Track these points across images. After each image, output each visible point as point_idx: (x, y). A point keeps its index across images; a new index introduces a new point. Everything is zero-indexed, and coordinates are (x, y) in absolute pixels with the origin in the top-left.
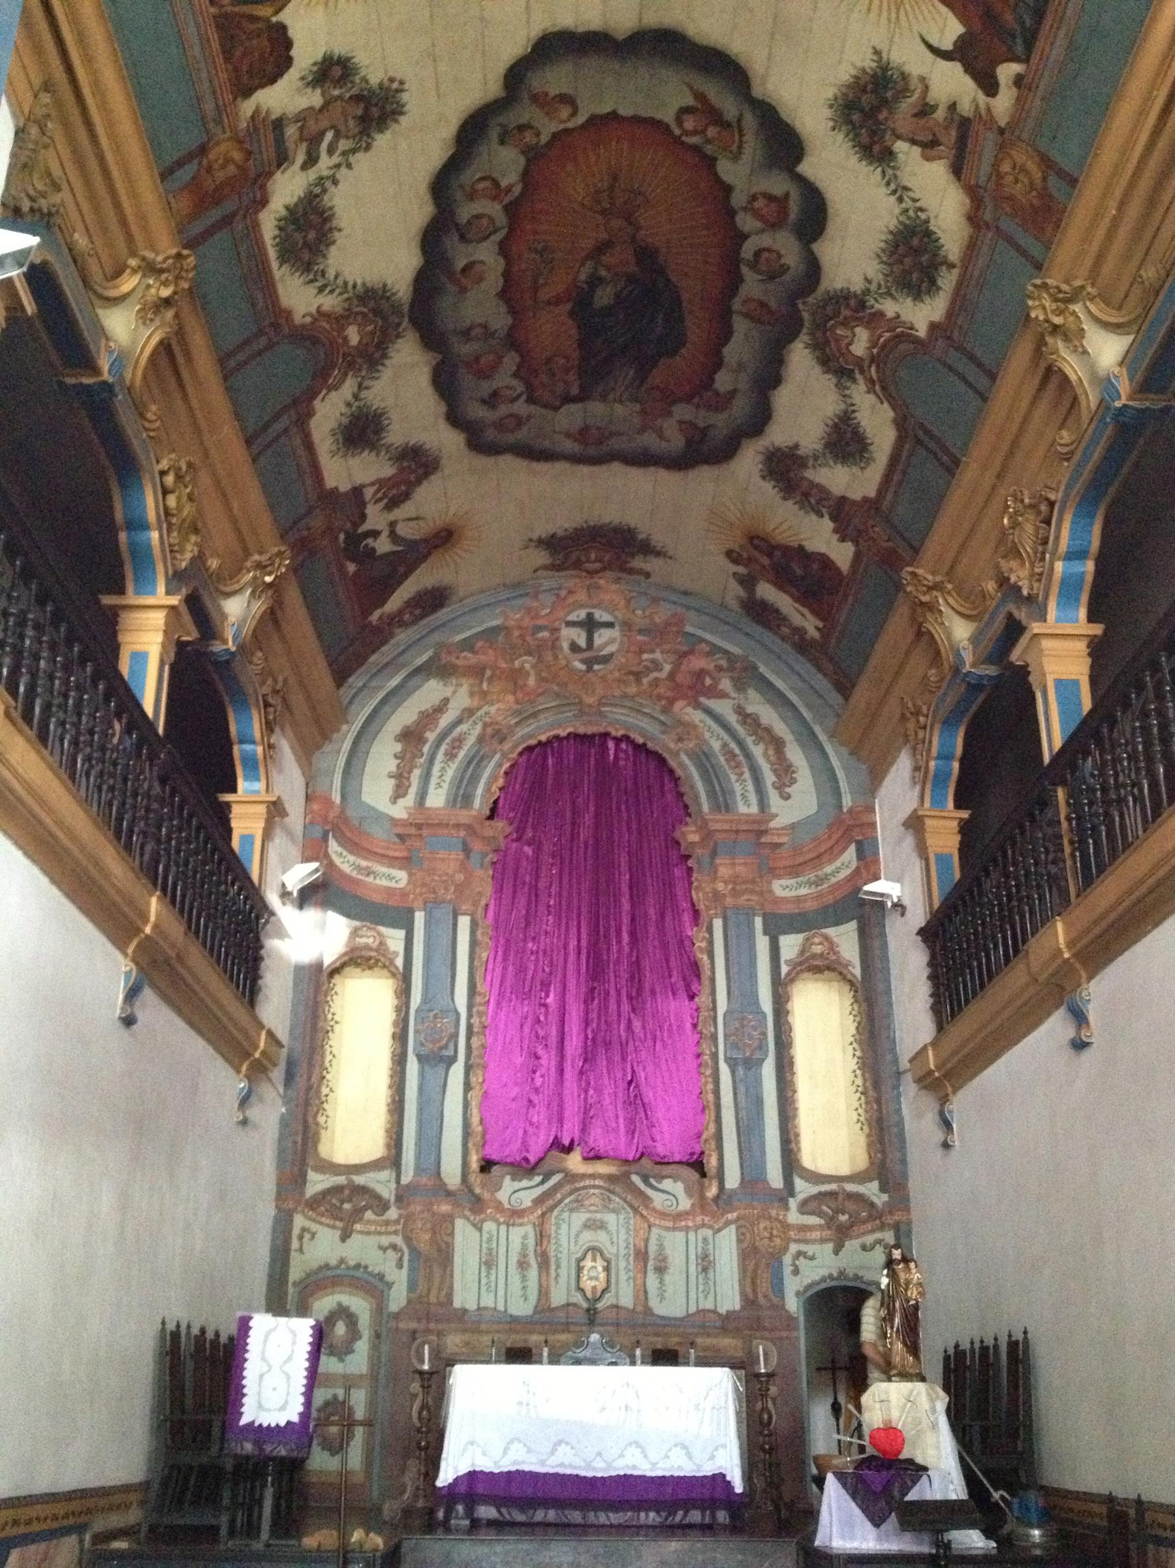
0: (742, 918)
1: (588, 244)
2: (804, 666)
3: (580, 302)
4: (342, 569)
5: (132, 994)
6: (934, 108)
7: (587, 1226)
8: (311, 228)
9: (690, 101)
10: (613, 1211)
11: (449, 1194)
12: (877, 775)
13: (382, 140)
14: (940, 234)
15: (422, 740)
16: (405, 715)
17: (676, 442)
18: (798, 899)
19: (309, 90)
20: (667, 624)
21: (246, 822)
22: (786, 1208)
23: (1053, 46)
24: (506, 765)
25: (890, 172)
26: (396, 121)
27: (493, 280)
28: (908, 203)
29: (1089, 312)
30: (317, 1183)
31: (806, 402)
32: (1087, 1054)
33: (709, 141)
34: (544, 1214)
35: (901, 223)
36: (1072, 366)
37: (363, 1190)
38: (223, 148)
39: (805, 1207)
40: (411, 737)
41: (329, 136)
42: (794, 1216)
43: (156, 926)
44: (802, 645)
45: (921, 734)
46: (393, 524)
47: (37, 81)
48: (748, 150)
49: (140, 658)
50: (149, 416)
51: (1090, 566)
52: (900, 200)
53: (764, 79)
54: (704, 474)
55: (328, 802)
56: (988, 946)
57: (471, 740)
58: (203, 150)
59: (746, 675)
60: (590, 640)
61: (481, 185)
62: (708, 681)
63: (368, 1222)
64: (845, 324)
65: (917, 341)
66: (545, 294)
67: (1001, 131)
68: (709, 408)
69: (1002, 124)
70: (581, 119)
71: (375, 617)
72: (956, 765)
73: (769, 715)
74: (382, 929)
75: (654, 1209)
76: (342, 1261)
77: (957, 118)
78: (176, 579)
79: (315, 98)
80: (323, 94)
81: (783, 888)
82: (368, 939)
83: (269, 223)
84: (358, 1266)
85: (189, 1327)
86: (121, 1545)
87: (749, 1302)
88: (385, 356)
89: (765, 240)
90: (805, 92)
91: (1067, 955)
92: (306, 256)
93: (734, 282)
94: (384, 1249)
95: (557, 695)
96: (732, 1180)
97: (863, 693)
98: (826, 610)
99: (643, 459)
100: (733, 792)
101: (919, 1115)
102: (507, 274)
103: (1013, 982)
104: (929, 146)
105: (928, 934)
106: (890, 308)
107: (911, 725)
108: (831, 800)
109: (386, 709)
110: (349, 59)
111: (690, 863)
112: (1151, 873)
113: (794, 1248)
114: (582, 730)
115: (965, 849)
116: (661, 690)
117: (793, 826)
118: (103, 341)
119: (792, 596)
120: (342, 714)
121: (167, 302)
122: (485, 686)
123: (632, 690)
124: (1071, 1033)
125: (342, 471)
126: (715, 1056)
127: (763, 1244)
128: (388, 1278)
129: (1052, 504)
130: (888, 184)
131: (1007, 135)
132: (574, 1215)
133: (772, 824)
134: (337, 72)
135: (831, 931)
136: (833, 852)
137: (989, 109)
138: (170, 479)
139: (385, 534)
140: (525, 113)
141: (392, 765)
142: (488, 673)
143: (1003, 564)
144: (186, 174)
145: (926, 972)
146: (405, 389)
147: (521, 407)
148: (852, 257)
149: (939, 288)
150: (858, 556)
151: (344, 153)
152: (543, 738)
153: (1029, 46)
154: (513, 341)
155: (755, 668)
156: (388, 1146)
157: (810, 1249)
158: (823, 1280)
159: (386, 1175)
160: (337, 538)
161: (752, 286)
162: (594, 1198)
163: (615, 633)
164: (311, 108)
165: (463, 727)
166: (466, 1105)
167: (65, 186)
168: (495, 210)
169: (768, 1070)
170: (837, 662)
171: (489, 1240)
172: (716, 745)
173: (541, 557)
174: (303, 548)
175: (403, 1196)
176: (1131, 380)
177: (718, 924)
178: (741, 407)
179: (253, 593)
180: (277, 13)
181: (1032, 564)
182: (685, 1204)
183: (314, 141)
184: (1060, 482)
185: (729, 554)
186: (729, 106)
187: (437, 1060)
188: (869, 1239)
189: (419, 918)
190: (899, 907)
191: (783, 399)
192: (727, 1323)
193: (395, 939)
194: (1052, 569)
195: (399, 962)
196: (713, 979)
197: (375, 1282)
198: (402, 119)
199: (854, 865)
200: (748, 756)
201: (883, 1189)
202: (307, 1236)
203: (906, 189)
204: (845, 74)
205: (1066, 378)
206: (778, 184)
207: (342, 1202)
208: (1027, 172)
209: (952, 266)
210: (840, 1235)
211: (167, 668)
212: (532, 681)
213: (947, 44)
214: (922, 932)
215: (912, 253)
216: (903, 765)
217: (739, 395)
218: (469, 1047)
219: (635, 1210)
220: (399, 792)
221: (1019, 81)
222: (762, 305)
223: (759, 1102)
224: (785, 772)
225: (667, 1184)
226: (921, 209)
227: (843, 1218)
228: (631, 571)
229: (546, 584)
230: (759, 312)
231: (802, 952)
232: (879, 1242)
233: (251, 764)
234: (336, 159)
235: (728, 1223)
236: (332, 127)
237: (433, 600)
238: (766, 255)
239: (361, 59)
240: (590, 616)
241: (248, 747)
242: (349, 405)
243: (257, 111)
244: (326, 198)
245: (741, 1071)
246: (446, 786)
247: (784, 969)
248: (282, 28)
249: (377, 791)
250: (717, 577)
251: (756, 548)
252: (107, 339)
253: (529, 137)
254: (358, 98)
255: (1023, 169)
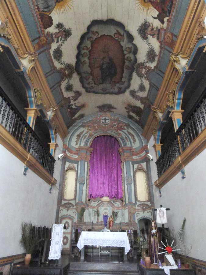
0: (128, 162)
1: (101, 57)
2: (137, 125)
3: (101, 67)
4: (68, 110)
5: (26, 170)
6: (154, 28)
7: (105, 209)
8: (58, 54)
9: (116, 32)
10: (108, 207)
11: (83, 204)
12: (148, 141)
13: (68, 39)
14: (155, 50)
15: (80, 136)
16: (78, 133)
17: (116, 90)
18: (137, 159)
19: (56, 29)
20: (116, 119)
21: (52, 147)
22: (135, 206)
23: (174, 13)
24: (92, 140)
25: (147, 41)
26: (71, 36)
27: (88, 64)
28: (150, 46)
29: (181, 57)
30: (63, 202)
31: (136, 82)
32: (185, 179)
33: (119, 39)
34: (98, 207)
35: (149, 50)
36: (177, 66)
37: (70, 203)
38: (43, 38)
39: (138, 206)
40: (79, 136)
41: (60, 37)
42: (137, 207)
43: (29, 159)
44: (137, 122)
45: (155, 133)
46: (75, 104)
47: (6, 16)
48: (125, 40)
49: (30, 118)
50: (32, 79)
51: (181, 101)
52: (149, 46)
53: (127, 26)
54: (121, 95)
55: (66, 146)
56: (167, 165)
57: (87, 136)
58: (39, 38)
59: (128, 126)
60: (105, 122)
61: (85, 48)
62: (123, 127)
63: (71, 208)
64: (141, 68)
65: (152, 70)
66: (96, 66)
67: (165, 30)
68: (121, 84)
69: (165, 29)
70: (100, 36)
71: (73, 118)
72: (160, 137)
73: (132, 132)
74: (74, 164)
75: (115, 207)
76: (67, 214)
77: (158, 30)
78: (37, 106)
79: (57, 31)
80: (59, 30)
81: (134, 157)
82: (72, 166)
83: (52, 51)
84: (69, 215)
85: (42, 226)
86: (18, 266)
87: (130, 221)
88: (72, 76)
89: (128, 55)
90: (133, 28)
91: (181, 162)
92: (58, 58)
93: (124, 63)
94: (73, 213)
95: (100, 130)
96: (127, 202)
97: (146, 127)
98: (140, 116)
99: (112, 93)
100: (127, 143)
101: (156, 191)
102: (90, 63)
103: (172, 168)
104: (153, 35)
105: (157, 163)
106: (148, 65)
107: (153, 131)
108: (141, 143)
109: (75, 132)
110: (62, 24)
111: (120, 154)
112: (197, 145)
113: (137, 212)
114: (104, 135)
115: (162, 150)
116: (116, 129)
117: (136, 148)
118: (22, 65)
119: (135, 114)
120: (69, 133)
121: (33, 60)
122: (90, 128)
123: (112, 128)
124: (182, 176)
125: (66, 94)
126: (124, 183)
127: (132, 212)
128: (74, 217)
129: (175, 91)
130: (147, 43)
131: (166, 31)
132: (103, 208)
133: (133, 148)
134: (60, 26)
135: (142, 164)
136: (142, 152)
137: (163, 27)
138: (36, 90)
139: (74, 105)
140: (91, 35)
141: (76, 140)
142: (90, 126)
143: (167, 103)
144: (36, 41)
145: (157, 169)
146: (75, 81)
147: (93, 85)
148: (142, 57)
149: (155, 60)
150: (144, 106)
151: (63, 41)
152: (98, 136)
153: (169, 14)
154: (91, 74)
155: (130, 125)
156: (74, 197)
157: (139, 213)
158: (141, 217)
159: (74, 201)
160: (66, 105)
161: (127, 63)
162: (106, 204)
163: (109, 120)
164: (57, 32)
165: (86, 134)
166: (86, 191)
167: (12, 35)
168: (87, 51)
169: (133, 185)
170: (141, 124)
171: (90, 211)
172: (124, 137)
173: (98, 109)
174: (61, 107)
175: (76, 204)
176: (188, 66)
177: (125, 163)
178: (126, 84)
179: (52, 111)
180: (50, 14)
181: (172, 102)
182: (120, 205)
183: (58, 38)
184: (176, 88)
185: (125, 108)
186: (122, 32)
187: (82, 183)
188: (148, 211)
189: (79, 162)
190: (152, 160)
191: (132, 82)
192: (127, 224)
193: (76, 165)
194: (175, 102)
195: (76, 169)
196: (124, 171)
197: (72, 218)
198: (72, 35)
199: (145, 154)
200: (129, 138)
201: (150, 203)
202: (62, 210)
203: (150, 44)
204: (140, 25)
205: (177, 70)
206: (130, 45)
207: (67, 205)
208: (170, 37)
209: (157, 56)
210: (144, 210)
211: (35, 120)
212: (96, 128)
213: (156, 16)
214: (156, 163)
215: (151, 55)
216: (152, 137)
217: (125, 82)
218: (87, 182)
219: (112, 207)
220: (77, 144)
221: (168, 20)
222: (128, 66)
223: (131, 190)
224: (134, 140)
225: (117, 203)
226: (152, 47)
227: (144, 208)
228: (111, 111)
229: (99, 114)
230: (128, 68)
231: (137, 167)
232: (150, 211)
233: (53, 138)
234: (62, 42)
235: (126, 209)
236: (61, 36)
237: (82, 116)
238: (128, 58)
239: (64, 24)
240: (105, 118)
241: (53, 136)
242: (67, 84)
243: (48, 32)
244: (61, 48)
245: (128, 185)
246: (83, 143)
247: (135, 170)
248: (50, 17)
249: (74, 144)
250: (124, 111)
251: (129, 107)
252: (23, 65)
253: (91, 39)
254: (64, 31)
255: (169, 36)
